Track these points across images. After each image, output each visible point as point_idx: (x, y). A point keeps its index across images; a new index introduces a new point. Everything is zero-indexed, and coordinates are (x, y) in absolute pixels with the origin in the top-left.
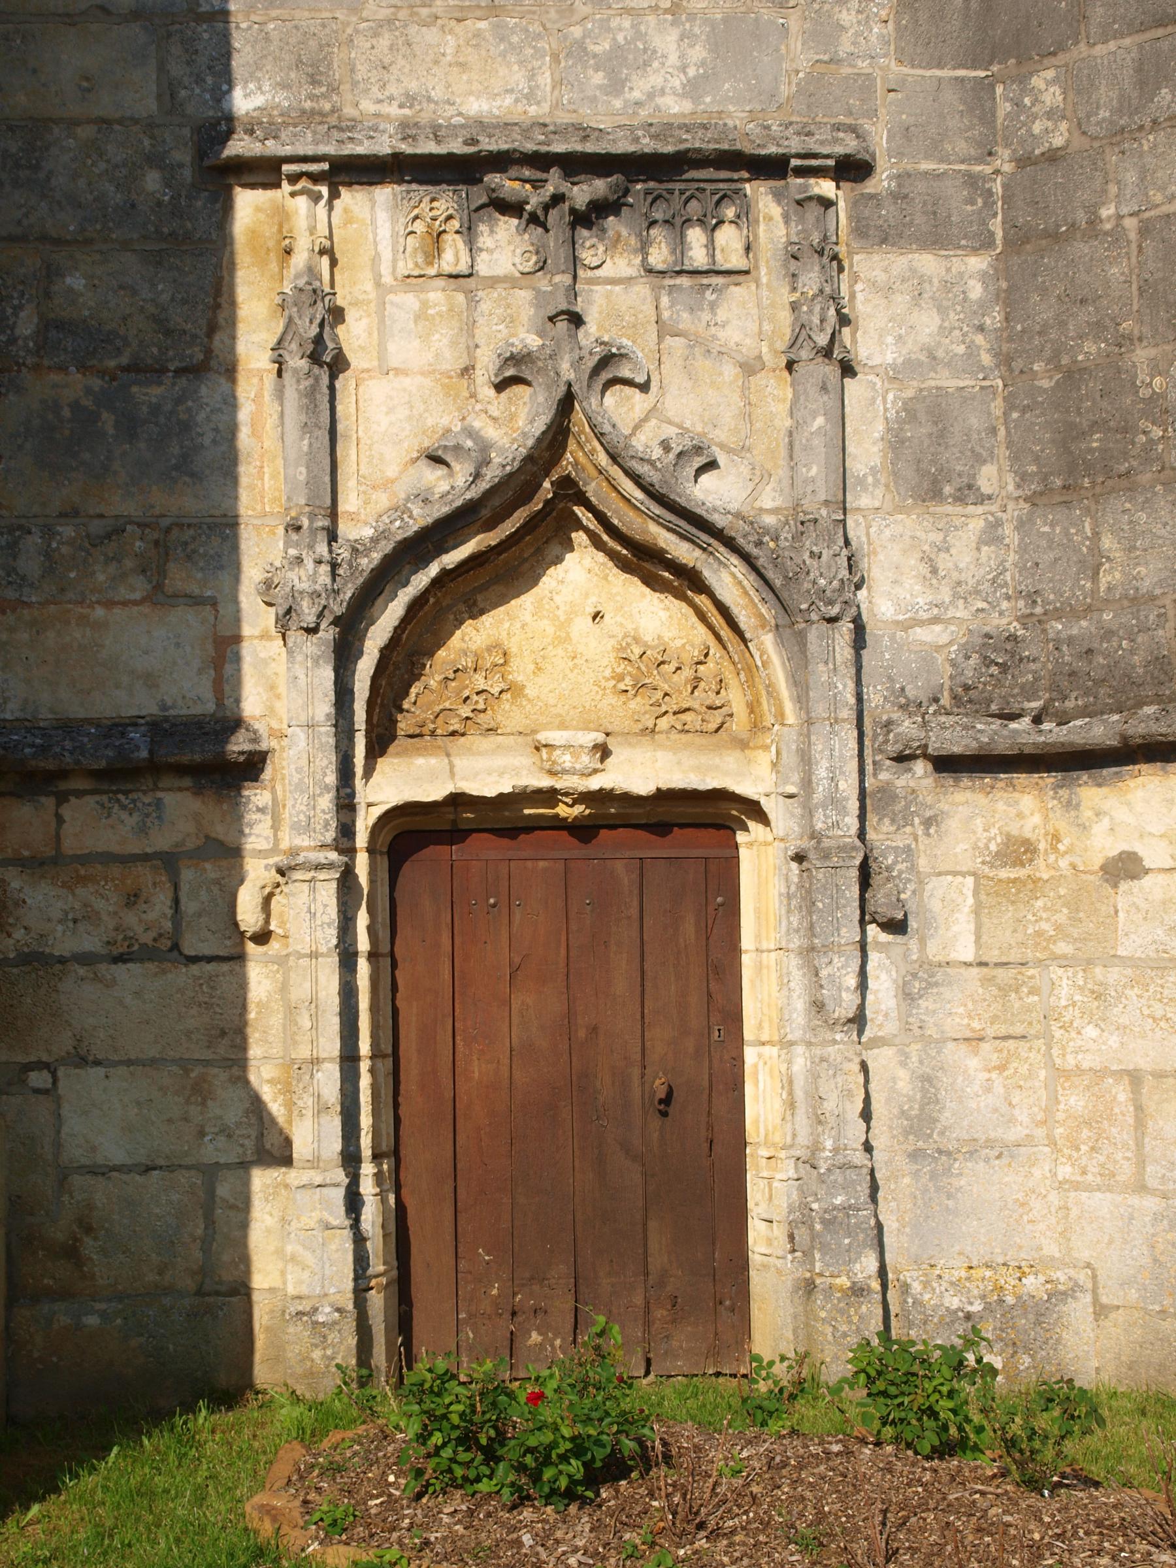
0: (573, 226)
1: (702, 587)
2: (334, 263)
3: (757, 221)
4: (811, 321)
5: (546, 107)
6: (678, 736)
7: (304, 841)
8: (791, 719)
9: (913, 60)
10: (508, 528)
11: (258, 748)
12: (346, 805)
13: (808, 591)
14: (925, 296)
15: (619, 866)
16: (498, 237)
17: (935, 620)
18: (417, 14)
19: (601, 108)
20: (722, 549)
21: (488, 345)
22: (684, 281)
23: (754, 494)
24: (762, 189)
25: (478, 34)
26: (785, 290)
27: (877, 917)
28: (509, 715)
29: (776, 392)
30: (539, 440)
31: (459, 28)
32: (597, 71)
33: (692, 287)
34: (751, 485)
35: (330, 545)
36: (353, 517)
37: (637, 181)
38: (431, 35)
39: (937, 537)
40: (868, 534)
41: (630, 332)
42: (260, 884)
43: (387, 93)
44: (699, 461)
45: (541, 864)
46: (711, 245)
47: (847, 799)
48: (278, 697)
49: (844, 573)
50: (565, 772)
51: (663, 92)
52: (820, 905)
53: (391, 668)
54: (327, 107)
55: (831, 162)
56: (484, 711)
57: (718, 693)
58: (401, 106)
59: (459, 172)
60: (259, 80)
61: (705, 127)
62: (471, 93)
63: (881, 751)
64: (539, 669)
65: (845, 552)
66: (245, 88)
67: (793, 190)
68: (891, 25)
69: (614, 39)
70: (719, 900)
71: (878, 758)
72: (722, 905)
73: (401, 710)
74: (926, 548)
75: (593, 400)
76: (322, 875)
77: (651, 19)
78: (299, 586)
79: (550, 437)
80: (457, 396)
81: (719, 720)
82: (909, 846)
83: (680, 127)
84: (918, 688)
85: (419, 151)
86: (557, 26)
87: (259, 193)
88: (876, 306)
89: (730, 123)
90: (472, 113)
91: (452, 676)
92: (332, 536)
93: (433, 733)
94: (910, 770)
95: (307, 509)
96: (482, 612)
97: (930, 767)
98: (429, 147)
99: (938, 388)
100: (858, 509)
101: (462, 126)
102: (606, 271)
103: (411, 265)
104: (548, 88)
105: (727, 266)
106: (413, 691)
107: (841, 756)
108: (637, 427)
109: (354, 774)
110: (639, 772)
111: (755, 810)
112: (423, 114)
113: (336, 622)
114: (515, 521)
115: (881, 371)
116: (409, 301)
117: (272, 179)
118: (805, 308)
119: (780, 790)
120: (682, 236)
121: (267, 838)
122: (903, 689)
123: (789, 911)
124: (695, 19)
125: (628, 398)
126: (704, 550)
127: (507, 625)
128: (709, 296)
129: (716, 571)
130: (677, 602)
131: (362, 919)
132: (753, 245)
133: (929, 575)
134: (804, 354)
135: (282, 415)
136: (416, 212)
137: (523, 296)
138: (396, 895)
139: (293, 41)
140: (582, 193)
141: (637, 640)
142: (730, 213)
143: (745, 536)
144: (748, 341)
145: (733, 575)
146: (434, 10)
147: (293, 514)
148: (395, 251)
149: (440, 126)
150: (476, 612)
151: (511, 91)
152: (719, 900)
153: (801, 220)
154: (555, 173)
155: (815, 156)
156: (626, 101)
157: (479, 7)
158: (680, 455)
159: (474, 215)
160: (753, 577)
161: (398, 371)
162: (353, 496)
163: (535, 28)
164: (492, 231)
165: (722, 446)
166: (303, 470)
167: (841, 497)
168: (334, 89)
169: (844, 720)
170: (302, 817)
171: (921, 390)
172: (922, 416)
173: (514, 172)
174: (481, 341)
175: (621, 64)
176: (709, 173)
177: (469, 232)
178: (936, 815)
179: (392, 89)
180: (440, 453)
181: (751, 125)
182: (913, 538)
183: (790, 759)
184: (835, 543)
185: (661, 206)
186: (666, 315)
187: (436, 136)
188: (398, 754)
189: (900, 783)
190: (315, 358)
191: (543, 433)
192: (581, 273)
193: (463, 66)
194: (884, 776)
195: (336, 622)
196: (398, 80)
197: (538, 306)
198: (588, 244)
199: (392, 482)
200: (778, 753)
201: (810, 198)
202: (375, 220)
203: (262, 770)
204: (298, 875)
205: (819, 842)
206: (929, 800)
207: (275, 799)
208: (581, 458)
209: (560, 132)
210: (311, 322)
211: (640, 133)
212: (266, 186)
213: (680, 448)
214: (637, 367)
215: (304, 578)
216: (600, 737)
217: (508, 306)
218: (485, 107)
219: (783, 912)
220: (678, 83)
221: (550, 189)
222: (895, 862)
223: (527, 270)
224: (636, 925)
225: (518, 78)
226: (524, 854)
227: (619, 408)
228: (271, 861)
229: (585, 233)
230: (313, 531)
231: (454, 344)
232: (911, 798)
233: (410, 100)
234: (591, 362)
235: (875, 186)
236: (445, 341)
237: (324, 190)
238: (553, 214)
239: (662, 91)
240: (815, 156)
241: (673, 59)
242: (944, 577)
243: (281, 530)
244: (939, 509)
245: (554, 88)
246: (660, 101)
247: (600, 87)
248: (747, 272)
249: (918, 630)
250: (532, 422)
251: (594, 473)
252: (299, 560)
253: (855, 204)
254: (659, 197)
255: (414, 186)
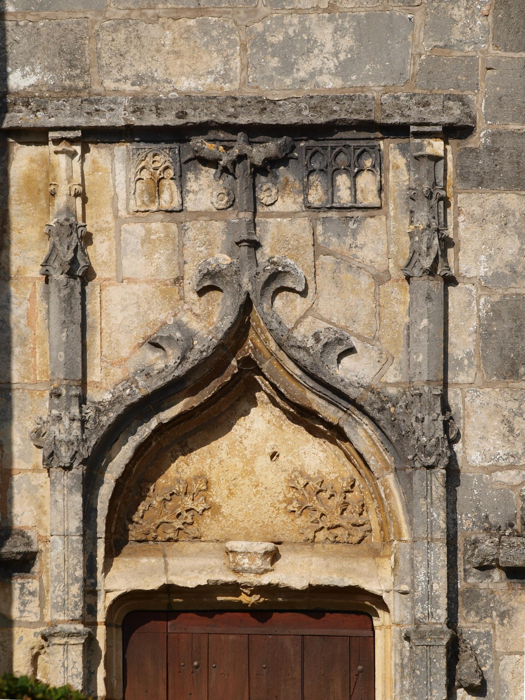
0: (254, 175)
1: (345, 439)
2: (85, 201)
3: (388, 169)
4: (420, 248)
5: (236, 85)
6: (331, 546)
7: (60, 616)
8: (406, 537)
9: (506, 45)
10: (206, 394)
11: (30, 550)
12: (90, 591)
13: (413, 446)
14: (510, 225)
15: (287, 641)
16: (201, 182)
17: (511, 467)
18: (144, 14)
19: (276, 85)
20: (357, 412)
21: (193, 261)
22: (334, 215)
23: (381, 372)
24: (392, 145)
25: (188, 29)
26: (407, 221)
27: (462, 683)
28: (210, 527)
29: (399, 299)
30: (227, 334)
31: (175, 25)
32: (273, 56)
33: (339, 219)
34: (379, 366)
35: (80, 407)
36: (97, 385)
37: (301, 140)
38: (155, 30)
39: (514, 405)
40: (464, 402)
41: (294, 253)
42: (30, 645)
43: (123, 74)
44: (340, 349)
45: (231, 637)
46: (354, 188)
47: (439, 597)
48: (45, 513)
49: (440, 433)
50: (244, 571)
51: (321, 72)
52: (418, 672)
53: (125, 491)
54: (81, 84)
55: (439, 129)
56: (192, 524)
57: (361, 514)
58: (133, 84)
59: (176, 137)
60: (32, 64)
61: (351, 98)
62: (183, 74)
63: (469, 562)
64: (231, 493)
65: (441, 418)
66: (22, 70)
67: (412, 147)
68: (490, 18)
69: (286, 33)
70: (360, 668)
71: (468, 567)
72: (362, 671)
73: (132, 522)
74: (506, 413)
75: (265, 305)
76: (72, 641)
77: (313, 16)
78: (59, 437)
79: (235, 329)
80: (171, 298)
81: (361, 535)
82: (489, 632)
83: (333, 99)
84: (498, 516)
85: (144, 124)
86: (245, 23)
87: (33, 147)
88: (473, 233)
89: (370, 95)
90: (184, 89)
91: (169, 498)
92: (82, 400)
93: (155, 539)
94: (490, 576)
95: (65, 382)
96: (191, 451)
97: (504, 575)
98: (152, 120)
99: (517, 295)
100: (457, 384)
101: (177, 100)
102: (278, 207)
103: (139, 203)
104: (238, 71)
105: (365, 203)
106: (141, 508)
107: (435, 565)
108: (298, 322)
109: (96, 569)
110: (297, 572)
111: (379, 602)
112: (149, 91)
113: (84, 462)
114: (213, 388)
115: (476, 281)
116: (138, 229)
117: (42, 140)
118: (417, 239)
119: (397, 588)
120: (333, 181)
121: (36, 614)
122: (487, 517)
123: (402, 677)
124: (345, 17)
125: (292, 301)
126: (345, 412)
127: (209, 461)
128: (352, 225)
129: (353, 428)
130: (332, 446)
131: (101, 673)
132: (384, 187)
133: (507, 434)
134: (416, 272)
135: (48, 312)
136: (143, 164)
137: (218, 226)
138: (126, 656)
139: (56, 35)
140: (258, 153)
141: (302, 474)
142: (368, 163)
143: (371, 405)
144: (379, 259)
145: (366, 432)
146: (157, 11)
147: (55, 384)
148: (128, 193)
149: (161, 99)
150: (186, 450)
151: (211, 73)
152: (360, 668)
153: (418, 170)
154: (241, 137)
155: (428, 124)
156: (294, 79)
157: (189, 9)
158: (326, 345)
159: (184, 166)
160: (378, 433)
161: (130, 280)
162: (97, 370)
163: (230, 24)
164: (197, 178)
165: (359, 336)
166: (62, 354)
167: (441, 376)
168: (85, 71)
169: (437, 540)
170: (59, 599)
171: (505, 296)
172: (505, 316)
173: (211, 135)
174: (188, 259)
175: (291, 52)
176: (353, 134)
177: (180, 179)
178: (508, 610)
179: (127, 72)
180: (158, 341)
181: (385, 97)
182: (496, 405)
183: (403, 565)
184: (434, 411)
185: (318, 158)
186: (320, 239)
187: (157, 109)
188: (129, 555)
189: (483, 586)
190: (71, 274)
191: (229, 329)
192: (260, 209)
193: (178, 54)
194: (471, 580)
195: (84, 462)
196: (131, 65)
197: (228, 234)
198: (264, 188)
199: (125, 360)
200: (396, 561)
201: (423, 156)
202: (113, 169)
203: (33, 565)
204: (56, 640)
205: (417, 627)
206: (504, 598)
207: (41, 586)
208: (260, 342)
209: (247, 105)
210: (68, 248)
211: (303, 105)
212: (37, 144)
213: (326, 340)
214: (297, 277)
215: (62, 431)
216: (270, 546)
217: (208, 233)
218: (193, 85)
219: (398, 677)
220: (332, 65)
221: (236, 151)
222: (478, 644)
223: (221, 207)
224: (299, 684)
225: (216, 62)
226: (218, 630)
227: (286, 308)
228: (38, 630)
229: (263, 179)
230: (69, 398)
231: (169, 260)
232: (490, 597)
233: (139, 79)
234: (264, 277)
235: (475, 143)
236: (163, 258)
237: (78, 149)
238: (239, 167)
239: (322, 68)
240: (428, 124)
241: (329, 47)
242: (518, 435)
243: (47, 394)
244: (516, 385)
245: (242, 70)
246: (319, 79)
247: (275, 69)
248: (380, 208)
249: (499, 474)
250: (222, 320)
251: (268, 355)
252: (59, 418)
253: (459, 156)
254: (316, 152)
255: (142, 144)
